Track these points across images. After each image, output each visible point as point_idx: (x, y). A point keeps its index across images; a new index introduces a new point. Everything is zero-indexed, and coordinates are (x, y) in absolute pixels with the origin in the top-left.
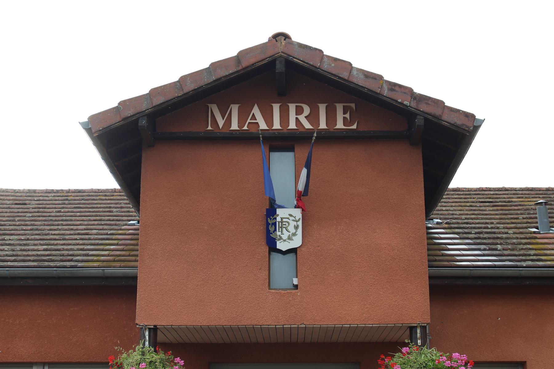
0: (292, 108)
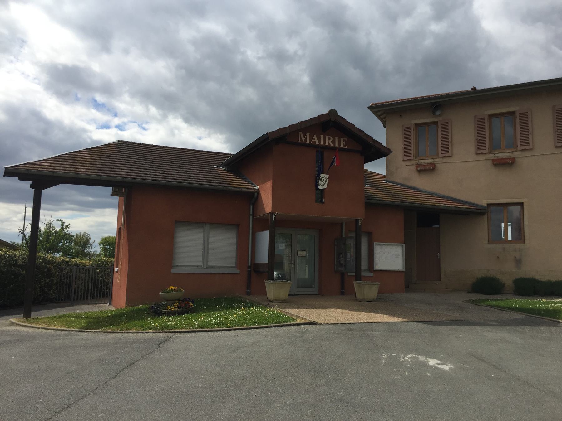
0: (327, 137)
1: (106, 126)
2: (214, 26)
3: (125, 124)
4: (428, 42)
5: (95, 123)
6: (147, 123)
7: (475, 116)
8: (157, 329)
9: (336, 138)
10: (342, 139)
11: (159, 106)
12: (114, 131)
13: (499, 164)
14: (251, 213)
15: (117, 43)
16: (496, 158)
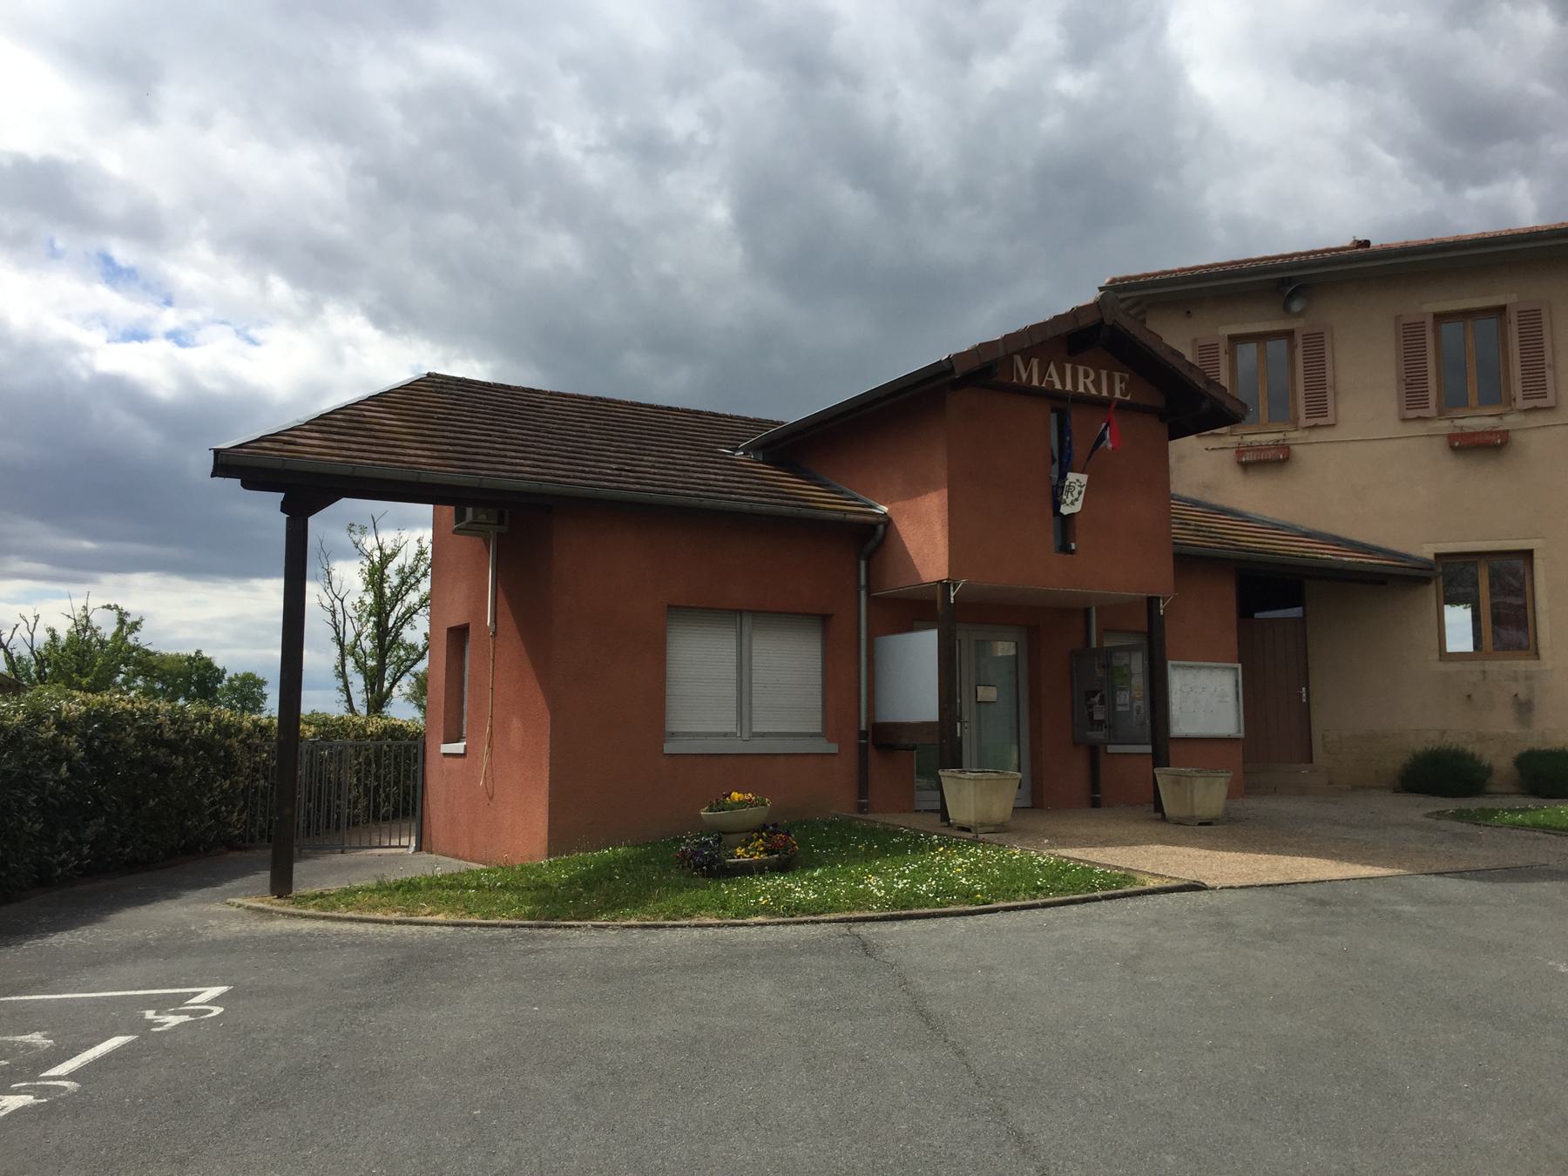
0: (1081, 369)
1: (138, 334)
2: (457, 57)
3: (197, 327)
4: (1052, 123)
5: (105, 325)
6: (261, 324)
7: (1397, 318)
8: (774, 914)
9: (1104, 373)
10: (1117, 375)
11: (300, 276)
12: (160, 348)
13: (1469, 446)
14: (863, 582)
15: (176, 97)
16: (1458, 431)
